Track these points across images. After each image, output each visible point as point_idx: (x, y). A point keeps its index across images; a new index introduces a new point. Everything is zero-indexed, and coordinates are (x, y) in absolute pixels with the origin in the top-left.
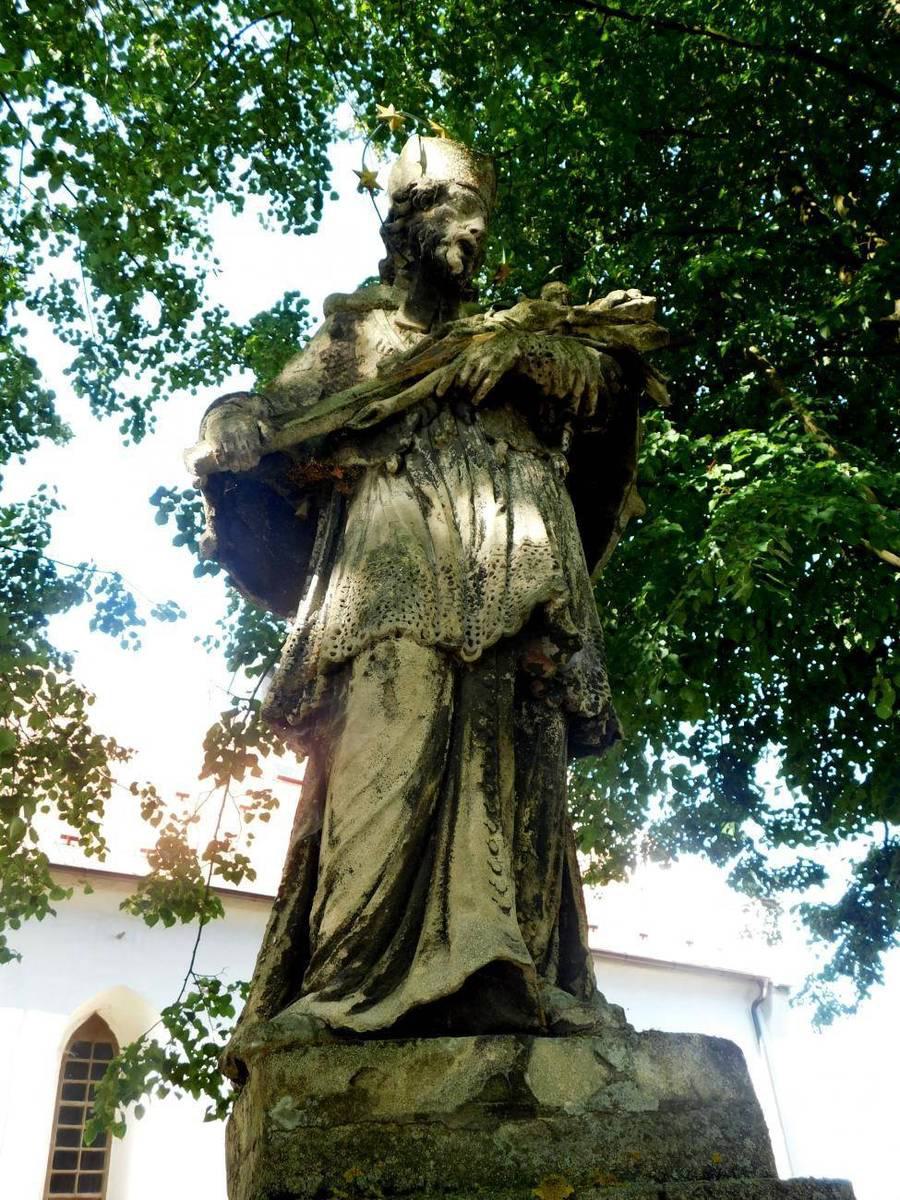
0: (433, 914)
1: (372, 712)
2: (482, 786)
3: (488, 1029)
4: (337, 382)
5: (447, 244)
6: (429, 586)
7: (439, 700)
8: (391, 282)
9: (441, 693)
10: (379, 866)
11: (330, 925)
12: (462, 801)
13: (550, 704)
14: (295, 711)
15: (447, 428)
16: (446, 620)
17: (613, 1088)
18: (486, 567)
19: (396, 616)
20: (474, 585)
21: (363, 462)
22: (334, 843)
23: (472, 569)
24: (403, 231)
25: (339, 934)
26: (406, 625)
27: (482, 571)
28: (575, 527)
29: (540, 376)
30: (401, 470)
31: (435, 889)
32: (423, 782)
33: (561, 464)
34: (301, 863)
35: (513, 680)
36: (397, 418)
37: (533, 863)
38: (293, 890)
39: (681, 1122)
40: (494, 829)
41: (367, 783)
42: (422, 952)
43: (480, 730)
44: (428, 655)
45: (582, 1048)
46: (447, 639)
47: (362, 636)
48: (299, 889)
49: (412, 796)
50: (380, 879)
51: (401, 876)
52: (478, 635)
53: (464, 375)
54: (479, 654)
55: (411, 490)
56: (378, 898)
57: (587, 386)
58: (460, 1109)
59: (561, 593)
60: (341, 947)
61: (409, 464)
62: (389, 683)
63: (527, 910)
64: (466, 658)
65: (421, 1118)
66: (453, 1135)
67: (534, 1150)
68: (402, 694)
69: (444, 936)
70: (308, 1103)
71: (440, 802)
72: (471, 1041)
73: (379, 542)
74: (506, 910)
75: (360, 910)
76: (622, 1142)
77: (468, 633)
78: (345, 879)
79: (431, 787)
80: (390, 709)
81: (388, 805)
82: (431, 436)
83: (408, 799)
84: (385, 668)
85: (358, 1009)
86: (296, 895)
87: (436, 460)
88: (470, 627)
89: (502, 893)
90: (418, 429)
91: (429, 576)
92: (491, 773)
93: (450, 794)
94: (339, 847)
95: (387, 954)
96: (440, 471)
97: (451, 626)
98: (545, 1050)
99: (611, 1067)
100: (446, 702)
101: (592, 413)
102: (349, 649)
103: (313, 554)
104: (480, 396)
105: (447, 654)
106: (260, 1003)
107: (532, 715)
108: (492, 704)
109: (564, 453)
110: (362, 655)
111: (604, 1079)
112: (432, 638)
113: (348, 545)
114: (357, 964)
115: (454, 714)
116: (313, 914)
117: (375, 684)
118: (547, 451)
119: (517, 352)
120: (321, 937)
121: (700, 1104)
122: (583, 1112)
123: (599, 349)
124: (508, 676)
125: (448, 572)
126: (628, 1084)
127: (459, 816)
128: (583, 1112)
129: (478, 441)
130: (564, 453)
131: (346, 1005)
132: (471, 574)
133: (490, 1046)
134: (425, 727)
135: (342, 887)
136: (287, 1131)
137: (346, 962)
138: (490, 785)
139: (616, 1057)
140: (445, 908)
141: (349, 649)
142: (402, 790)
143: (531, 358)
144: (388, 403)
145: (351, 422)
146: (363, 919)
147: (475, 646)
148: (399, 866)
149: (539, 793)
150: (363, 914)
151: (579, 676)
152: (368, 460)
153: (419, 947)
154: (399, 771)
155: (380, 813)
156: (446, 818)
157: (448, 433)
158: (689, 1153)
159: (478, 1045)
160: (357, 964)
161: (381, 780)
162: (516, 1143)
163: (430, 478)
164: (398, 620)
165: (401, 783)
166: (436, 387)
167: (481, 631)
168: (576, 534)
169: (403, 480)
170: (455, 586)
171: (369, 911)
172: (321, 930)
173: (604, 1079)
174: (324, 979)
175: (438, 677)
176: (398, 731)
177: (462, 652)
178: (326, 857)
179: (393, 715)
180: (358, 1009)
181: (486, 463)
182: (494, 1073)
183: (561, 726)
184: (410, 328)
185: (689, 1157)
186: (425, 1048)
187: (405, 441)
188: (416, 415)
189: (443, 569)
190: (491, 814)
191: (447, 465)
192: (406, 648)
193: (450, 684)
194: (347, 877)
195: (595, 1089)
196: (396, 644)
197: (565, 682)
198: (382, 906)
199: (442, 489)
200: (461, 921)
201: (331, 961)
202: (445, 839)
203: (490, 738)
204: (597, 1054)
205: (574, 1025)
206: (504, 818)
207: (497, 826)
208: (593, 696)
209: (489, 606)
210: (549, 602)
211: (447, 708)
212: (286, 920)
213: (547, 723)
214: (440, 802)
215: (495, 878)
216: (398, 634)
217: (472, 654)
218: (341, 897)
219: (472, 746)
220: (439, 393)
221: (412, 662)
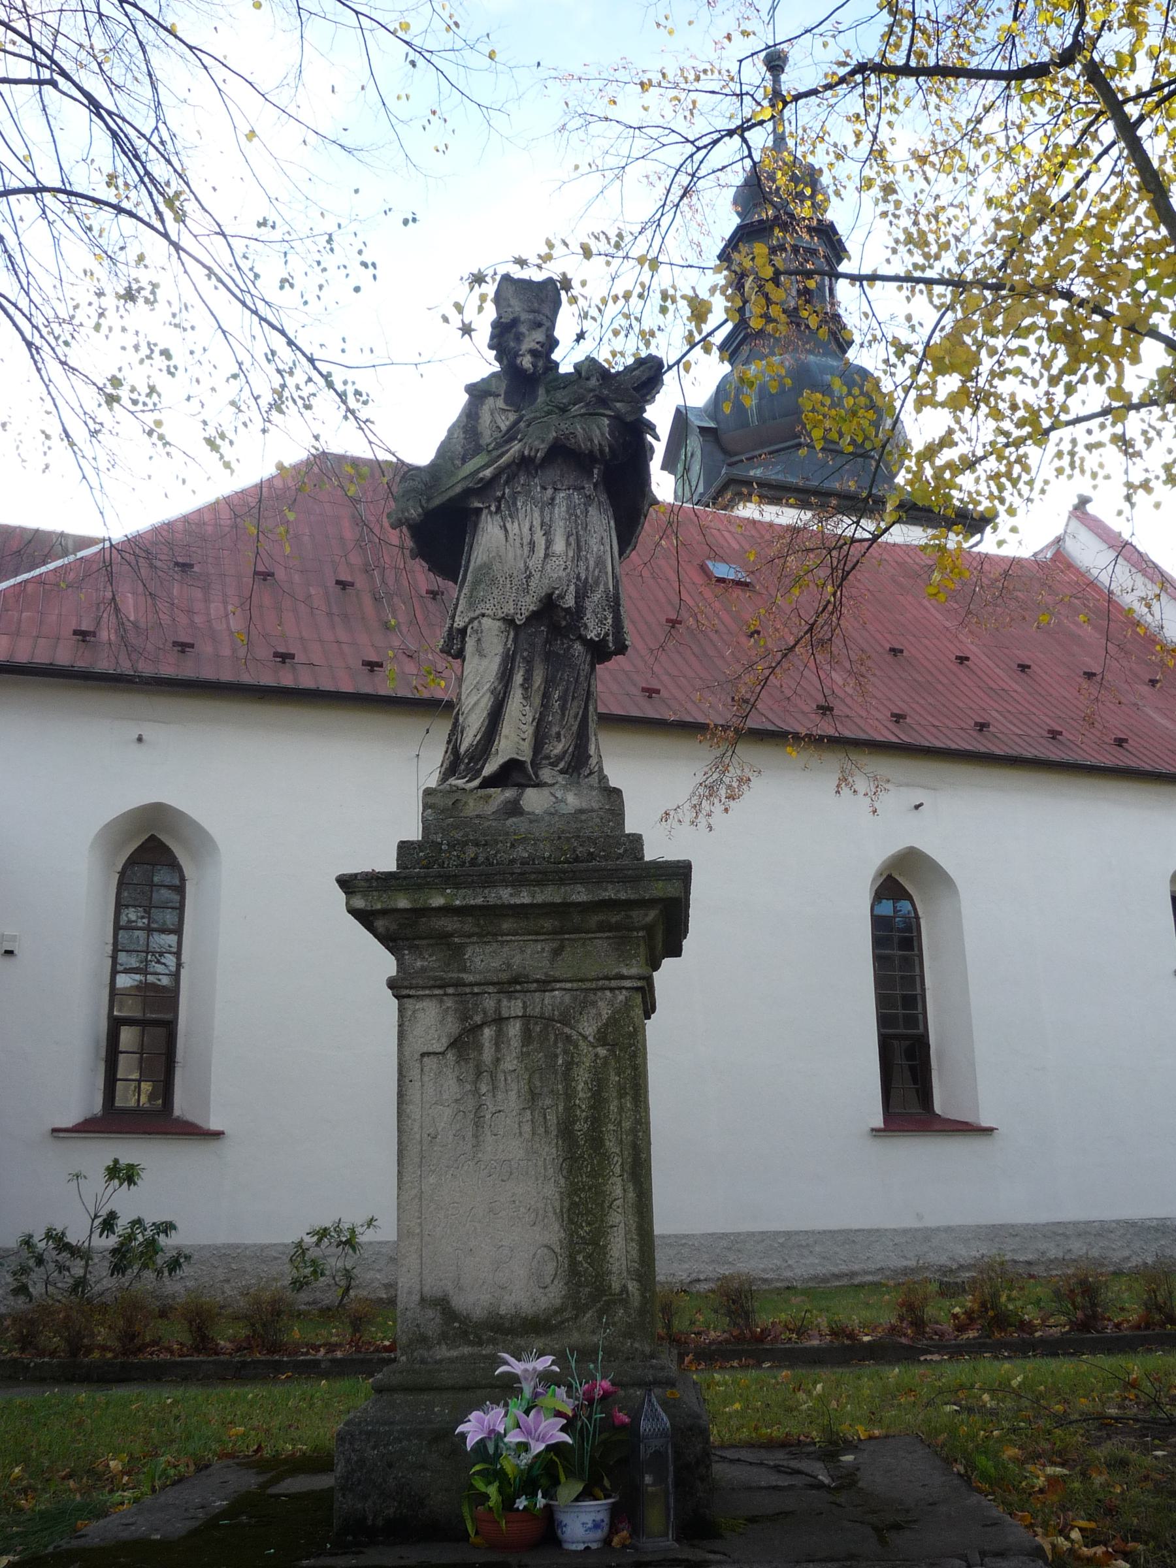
2: (522, 685)
5: (523, 355)
7: (506, 644)
21: (481, 505)
25: (467, 750)
37: (558, 717)
39: (583, 817)
43: (524, 658)
44: (499, 624)
45: (546, 791)
56: (478, 737)
62: (479, 640)
65: (478, 816)
68: (485, 645)
80: (481, 653)
81: (482, 697)
90: (507, 482)
92: (528, 679)
97: (509, 609)
98: (530, 793)
104: (538, 461)
105: (509, 621)
108: (532, 645)
134: (498, 659)
137: (468, 763)
138: (527, 685)
139: (559, 795)
165: (488, 685)
176: (485, 662)
187: (499, 494)
199: (516, 524)
203: (529, 662)
210: (553, 593)
216: (483, 615)
221: (490, 629)
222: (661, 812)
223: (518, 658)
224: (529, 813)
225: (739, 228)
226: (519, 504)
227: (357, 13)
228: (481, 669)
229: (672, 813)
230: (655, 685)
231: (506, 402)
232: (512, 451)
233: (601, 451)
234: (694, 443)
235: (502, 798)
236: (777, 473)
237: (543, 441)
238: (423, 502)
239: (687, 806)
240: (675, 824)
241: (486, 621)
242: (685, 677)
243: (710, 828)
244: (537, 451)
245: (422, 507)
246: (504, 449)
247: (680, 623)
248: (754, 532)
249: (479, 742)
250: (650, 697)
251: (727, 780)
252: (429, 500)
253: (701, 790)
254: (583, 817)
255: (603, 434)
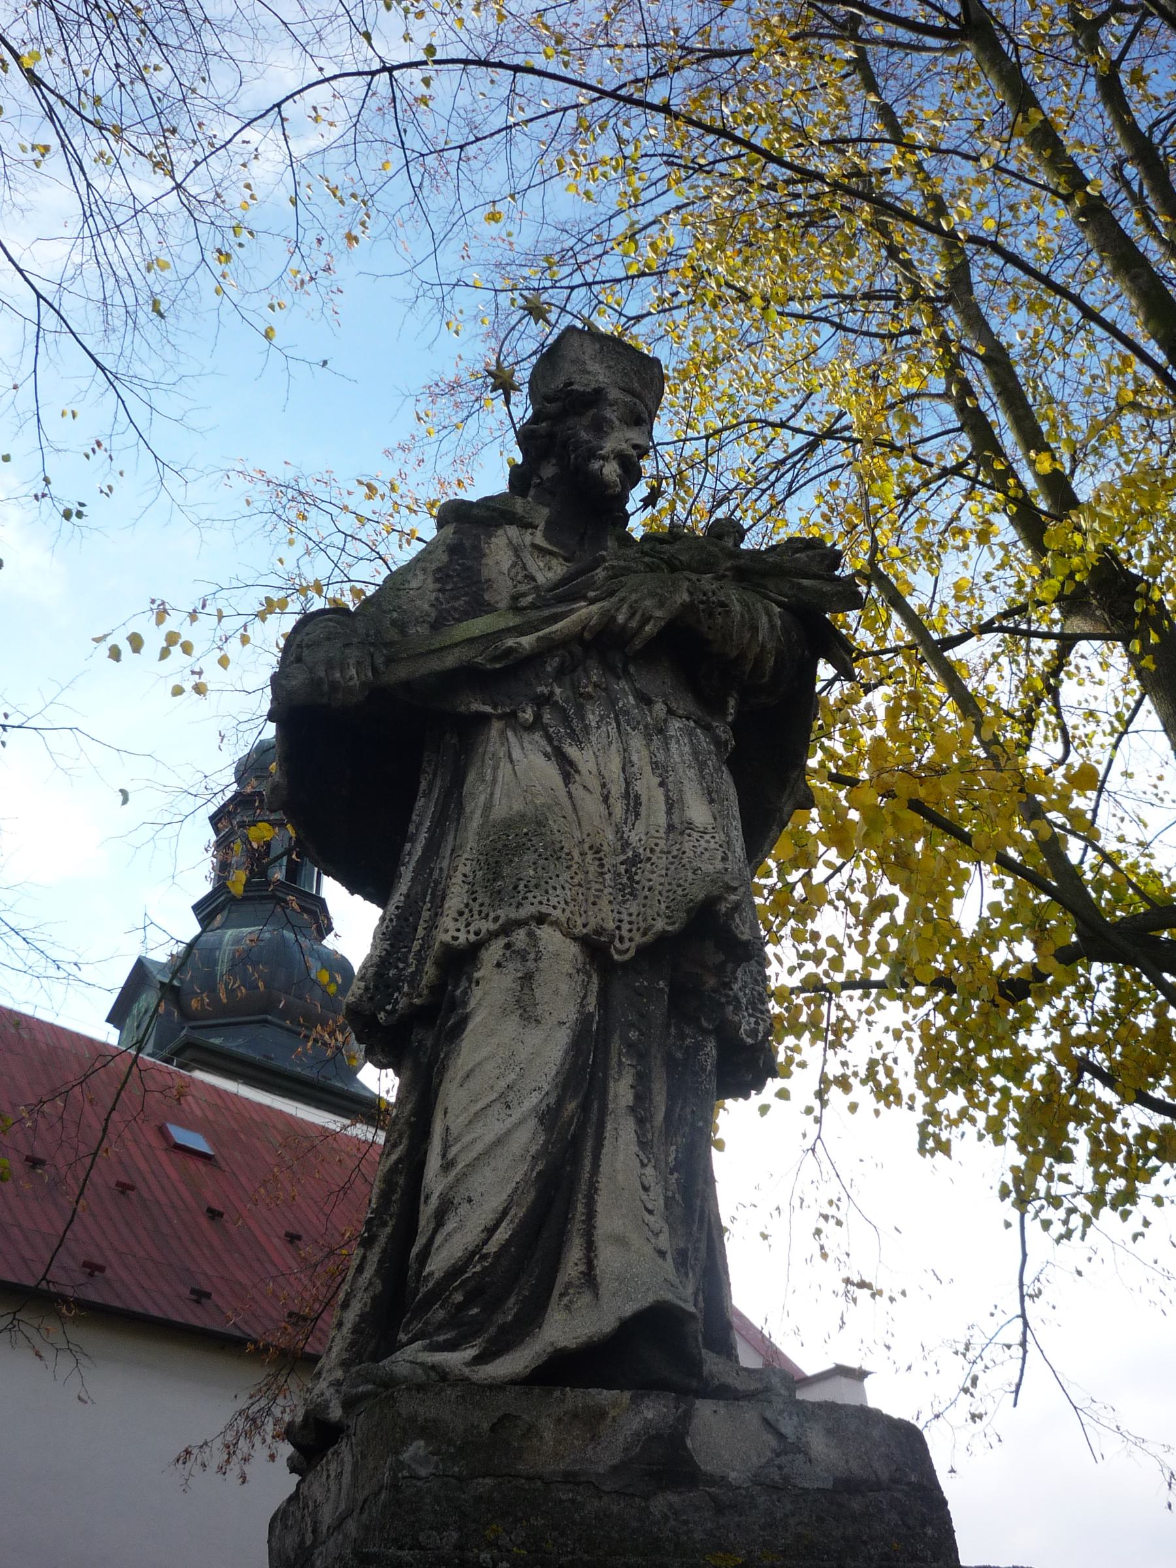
0: (575, 1254)
1: (505, 1012)
2: (632, 1109)
3: (646, 1385)
4: (456, 609)
5: (604, 458)
6: (575, 866)
7: (582, 1006)
8: (524, 495)
9: (584, 997)
10: (505, 1196)
11: (437, 1265)
12: (609, 1126)
13: (705, 1024)
14: (389, 1007)
15: (595, 678)
16: (596, 908)
17: (783, 1459)
18: (641, 850)
19: (539, 898)
20: (626, 871)
21: (488, 709)
22: (447, 1166)
23: (624, 852)
24: (551, 435)
25: (455, 1271)
26: (551, 910)
27: (636, 855)
28: (738, 815)
29: (710, 628)
30: (537, 724)
31: (577, 1227)
32: (560, 1103)
33: (724, 733)
34: (394, 1192)
35: (667, 989)
36: (535, 659)
38: (385, 1224)
39: (856, 1505)
40: (646, 1161)
41: (495, 1096)
42: (562, 1295)
43: (630, 1045)
45: (750, 1415)
46: (596, 932)
47: (496, 919)
48: (391, 1223)
49: (548, 1117)
50: (505, 1213)
51: (532, 1209)
52: (630, 931)
53: (621, 618)
54: (632, 953)
55: (549, 749)
56: (503, 1234)
57: (763, 647)
58: (615, 1469)
59: (735, 889)
60: (456, 1289)
61: (547, 717)
62: (527, 978)
63: (682, 1260)
64: (616, 957)
65: (570, 1478)
66: (605, 1499)
67: (695, 1522)
69: (590, 1279)
70: (444, 1448)
71: (582, 1126)
72: (627, 1395)
73: (511, 808)
74: (662, 1254)
75: (478, 1248)
76: (792, 1521)
77: (619, 928)
78: (461, 1211)
79: (571, 1106)
81: (519, 1124)
82: (575, 687)
83: (541, 1120)
84: (524, 959)
85: (478, 1360)
86: (388, 1230)
87: (582, 718)
88: (620, 921)
89: (657, 1235)
91: (576, 854)
92: (642, 1097)
93: (594, 1117)
94: (453, 1174)
95: (512, 1300)
96: (586, 729)
97: (605, 915)
98: (704, 1409)
99: (781, 1436)
100: (591, 1009)
101: (766, 679)
102: (477, 934)
103: (414, 817)
104: (638, 643)
106: (345, 1356)
107: (682, 1036)
109: (729, 723)
110: (493, 942)
111: (773, 1451)
112: (579, 930)
113: (468, 809)
114: (475, 1311)
115: (598, 1023)
116: (415, 1250)
117: (510, 978)
118: (708, 719)
119: (686, 597)
120: (426, 1279)
121: (877, 1486)
122: (749, 1484)
123: (779, 604)
124: (662, 984)
125: (597, 852)
126: (801, 1457)
127: (606, 1142)
128: (749, 1484)
129: (631, 698)
130: (729, 723)
131: (469, 1353)
132: (623, 857)
133: (647, 1401)
134: (563, 1038)
135: (457, 1219)
136: (420, 1479)
140: (590, 1247)
141: (477, 934)
142: (535, 1109)
143: (701, 606)
144: (527, 641)
145: (479, 660)
146: (484, 1257)
147: (627, 944)
148: (530, 1197)
149: (687, 1129)
150: (484, 1251)
151: (741, 994)
152: (495, 708)
153: (556, 1293)
154: (534, 1085)
155: (509, 1132)
156: (589, 1144)
157: (596, 686)
158: (865, 1538)
159: (633, 1400)
160: (475, 1311)
161: (512, 1094)
162: (675, 1513)
163: (573, 735)
164: (541, 903)
165: (535, 1098)
166: (584, 629)
167: (635, 927)
168: (737, 823)
169: (537, 736)
170: (606, 869)
171: (492, 1247)
172: (427, 1270)
173: (773, 1451)
174: (430, 1328)
175: (582, 977)
176: (534, 1037)
177: (613, 951)
178: (434, 1181)
179: (529, 1018)
180: (478, 1360)
181: (641, 727)
182: (652, 1432)
183: (714, 1052)
184: (551, 553)
185: (865, 1543)
186: (574, 1398)
188: (557, 659)
189: (591, 848)
190: (643, 1144)
191: (593, 724)
192: (549, 937)
193: (594, 987)
194: (464, 1208)
195: (763, 1460)
196: (538, 932)
197: (723, 1000)
198: (509, 1242)
200: (608, 1259)
201: (441, 1307)
202: (588, 1168)
203: (640, 1053)
204: (766, 1422)
205: (736, 1390)
206: (655, 1150)
207: (649, 1158)
208: (752, 1020)
209: (646, 897)
210: (720, 898)
211: (591, 1015)
212: (376, 1259)
213: (699, 1047)
214: (582, 1126)
215: (647, 1217)
216: (541, 919)
217: (624, 950)
218: (455, 1230)
219: (620, 1063)
220: (586, 635)
222: (179, 1450)
223: (616, 1043)
224: (711, 1480)
225: (237, 794)
226: (592, 719)
227: (39, 296)
228: (523, 1054)
229: (195, 1451)
230: (98, 1260)
231: (547, 536)
232: (574, 617)
233: (759, 661)
234: (148, 999)
235: (636, 1424)
236: (238, 1046)
237: (661, 605)
238: (379, 660)
239: (218, 1444)
240: (197, 1469)
241: (549, 937)
242: (134, 1256)
243: (244, 1479)
244: (646, 620)
245: (374, 669)
246: (547, 612)
247: (132, 1188)
248: (219, 1102)
249: (504, 1247)
250: (91, 1275)
251: (277, 1411)
252: (390, 660)
253: (241, 1422)
254: (856, 1505)
255: (772, 626)
